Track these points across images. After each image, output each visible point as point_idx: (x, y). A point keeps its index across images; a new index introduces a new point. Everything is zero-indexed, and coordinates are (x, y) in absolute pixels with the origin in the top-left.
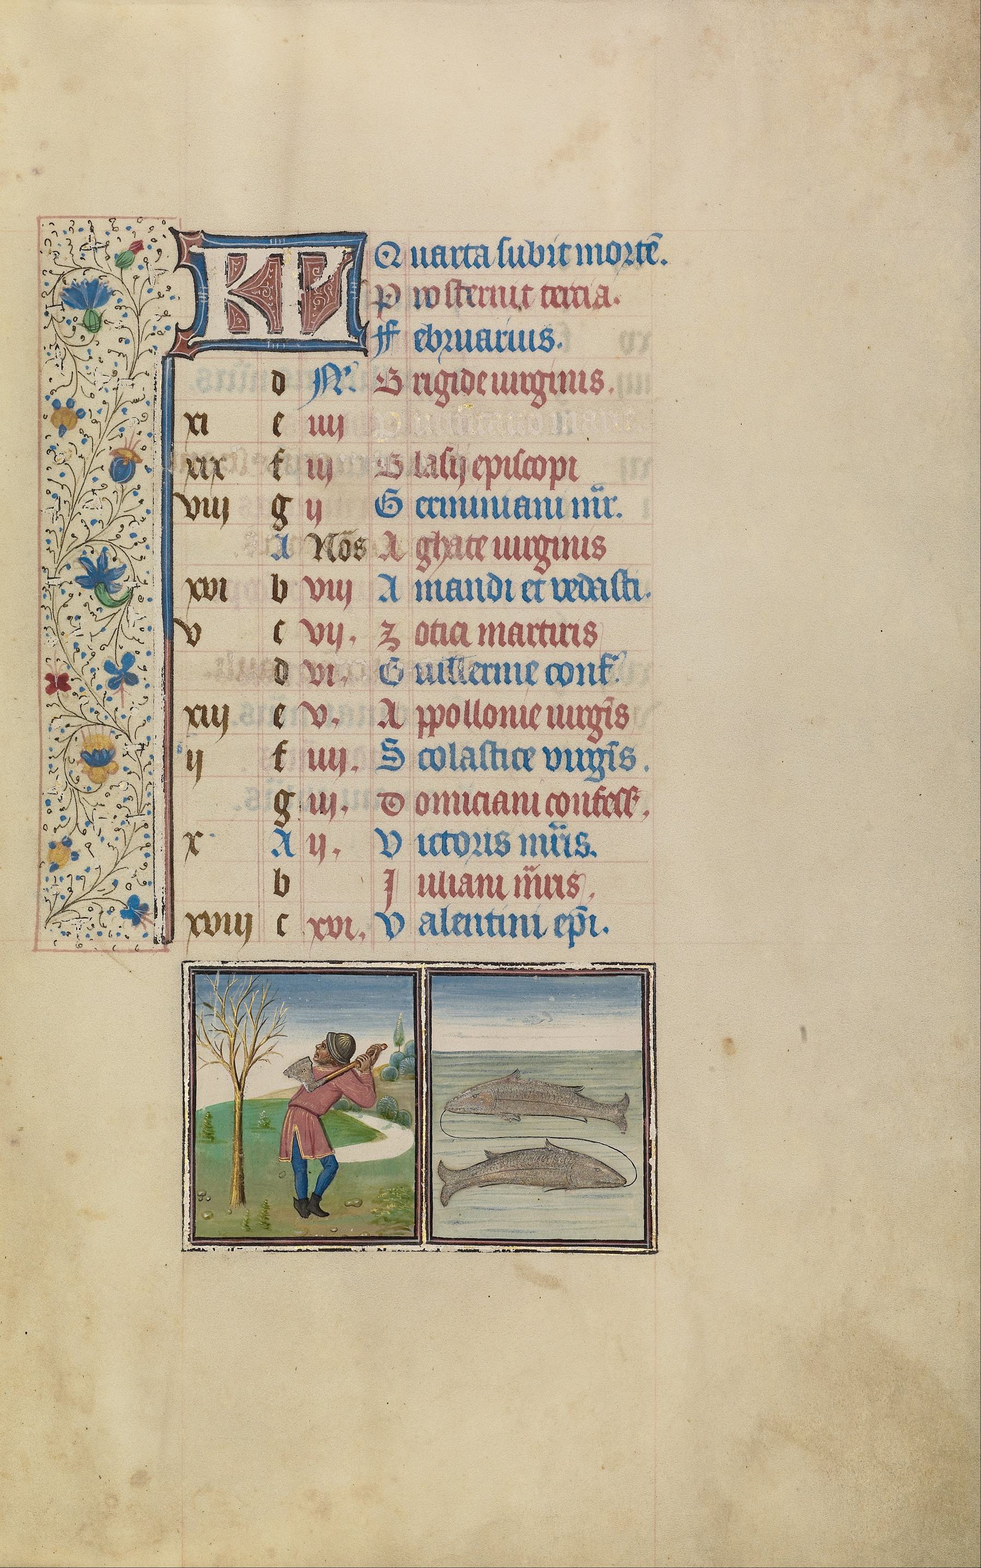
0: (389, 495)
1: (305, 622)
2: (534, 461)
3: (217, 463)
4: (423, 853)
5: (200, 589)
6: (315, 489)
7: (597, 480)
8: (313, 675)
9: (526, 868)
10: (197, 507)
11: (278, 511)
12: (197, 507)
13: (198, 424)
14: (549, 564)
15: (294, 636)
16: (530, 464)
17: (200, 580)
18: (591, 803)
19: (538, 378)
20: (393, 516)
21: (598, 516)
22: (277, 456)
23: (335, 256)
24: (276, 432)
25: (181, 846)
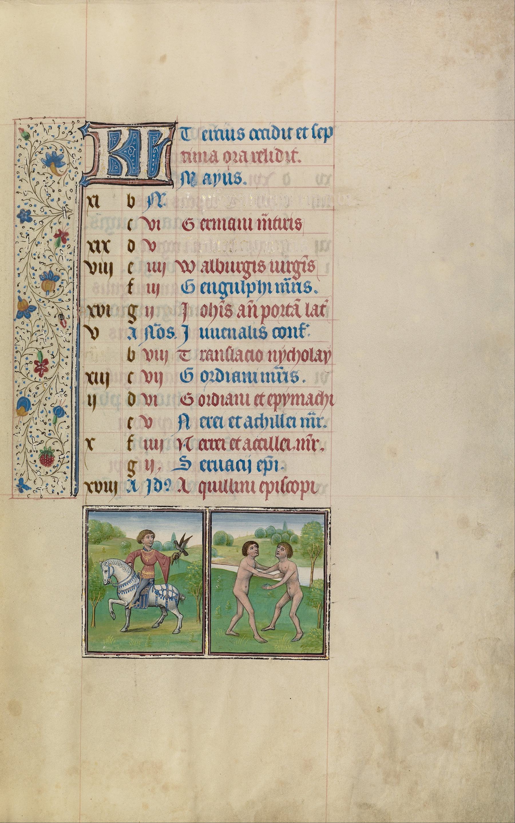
0: (188, 371)
2: (293, 483)
4: (202, 337)
6: (150, 300)
9: (286, 279)
10: (93, 268)
12: (93, 268)
14: (299, 276)
15: (140, 226)
16: (290, 485)
22: (130, 282)
24: (129, 427)
25: (83, 445)
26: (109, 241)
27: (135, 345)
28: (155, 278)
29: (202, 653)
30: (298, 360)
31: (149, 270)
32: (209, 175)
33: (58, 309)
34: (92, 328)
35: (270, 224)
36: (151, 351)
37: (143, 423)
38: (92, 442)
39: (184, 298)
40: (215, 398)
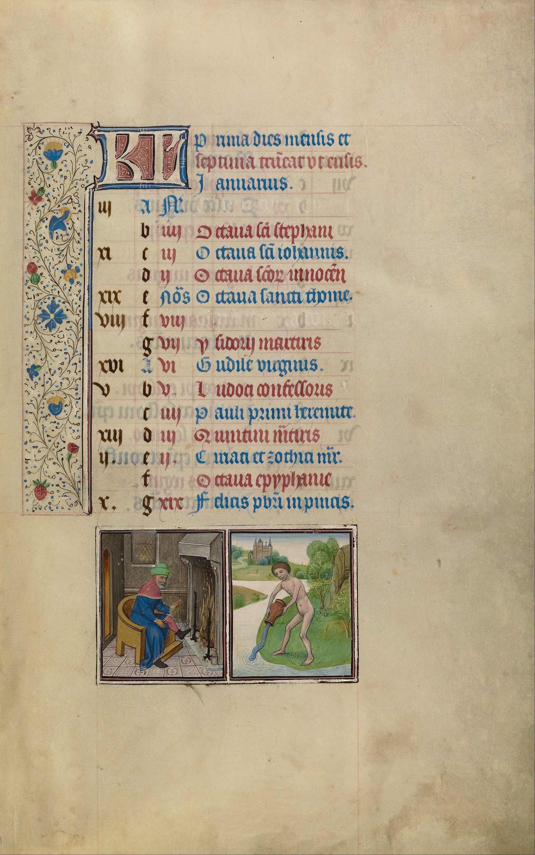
1: (160, 359)
3: (116, 294)
5: (106, 436)
6: (166, 265)
7: (331, 443)
8: (164, 390)
11: (146, 504)
13: (105, 253)
17: (106, 361)
18: (282, 389)
19: (282, 364)
20: (200, 270)
21: (330, 462)
23: (176, 134)
24: (145, 302)
26: (120, 291)
27: (151, 379)
28: (169, 425)
29: (224, 678)
30: (307, 237)
31: (163, 440)
32: (222, 180)
33: (63, 426)
34: (103, 385)
35: (279, 390)
36: (168, 362)
37: (161, 367)
38: (106, 501)
39: (200, 377)
40: (231, 388)
